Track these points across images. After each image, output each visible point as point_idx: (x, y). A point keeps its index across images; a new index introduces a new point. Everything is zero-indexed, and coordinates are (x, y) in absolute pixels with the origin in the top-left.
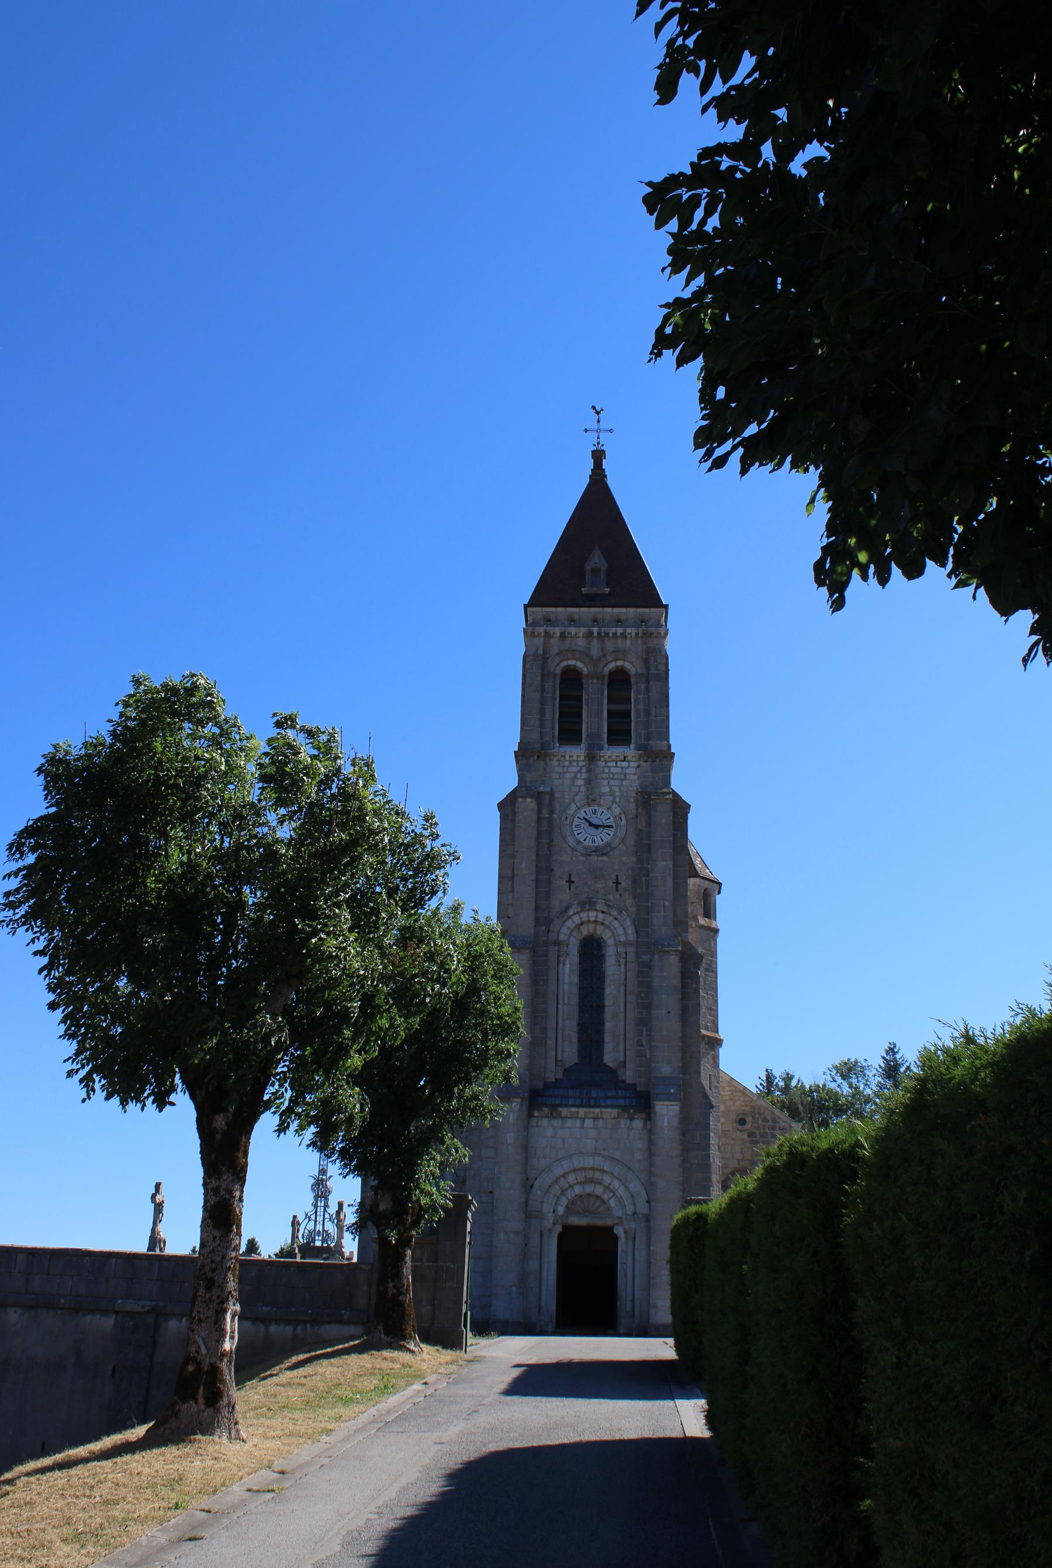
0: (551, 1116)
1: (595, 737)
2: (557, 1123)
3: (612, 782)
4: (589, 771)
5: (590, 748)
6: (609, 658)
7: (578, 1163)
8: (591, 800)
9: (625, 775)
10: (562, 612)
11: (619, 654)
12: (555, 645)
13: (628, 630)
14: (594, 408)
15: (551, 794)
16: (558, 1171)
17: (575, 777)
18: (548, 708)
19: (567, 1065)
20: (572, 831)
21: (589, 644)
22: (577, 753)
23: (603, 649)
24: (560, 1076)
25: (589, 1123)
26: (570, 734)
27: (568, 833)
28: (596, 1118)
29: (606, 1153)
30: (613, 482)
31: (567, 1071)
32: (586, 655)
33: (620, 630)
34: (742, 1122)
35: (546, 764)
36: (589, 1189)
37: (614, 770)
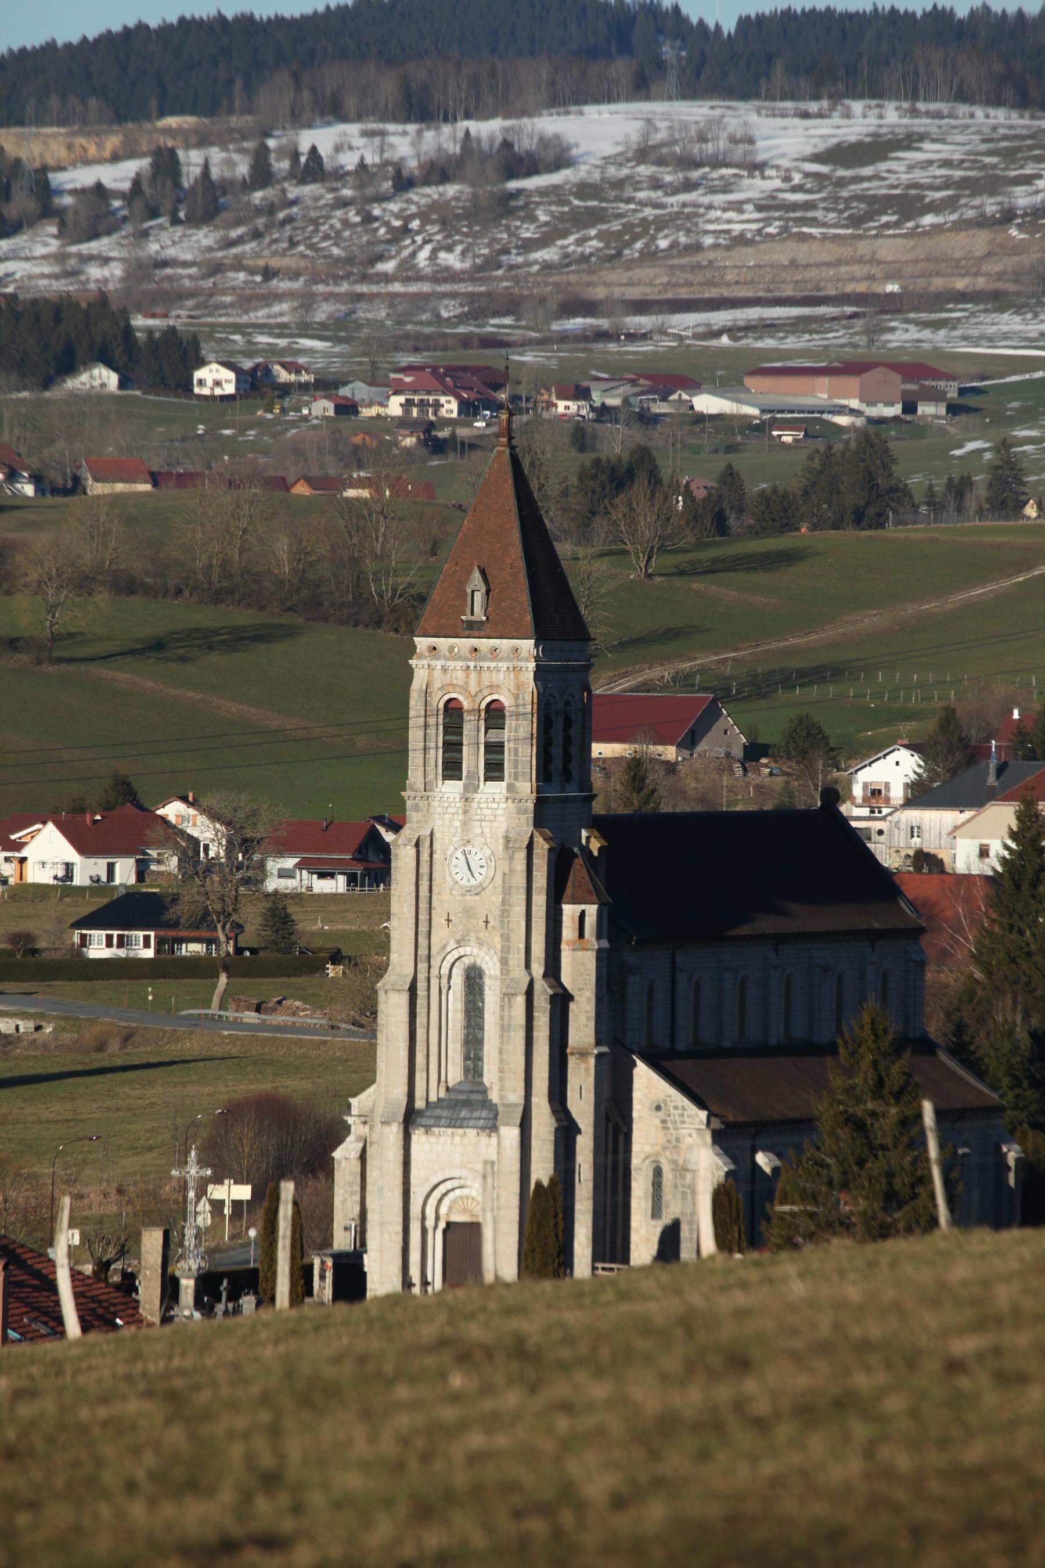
2: (432, 1139)
3: (483, 824)
4: (465, 812)
5: (466, 788)
6: (485, 692)
9: (495, 816)
11: (494, 687)
13: (500, 664)
17: (453, 819)
21: (467, 677)
23: (479, 682)
27: (447, 874)
29: (470, 1166)
33: (493, 665)
35: (429, 804)
37: (485, 812)
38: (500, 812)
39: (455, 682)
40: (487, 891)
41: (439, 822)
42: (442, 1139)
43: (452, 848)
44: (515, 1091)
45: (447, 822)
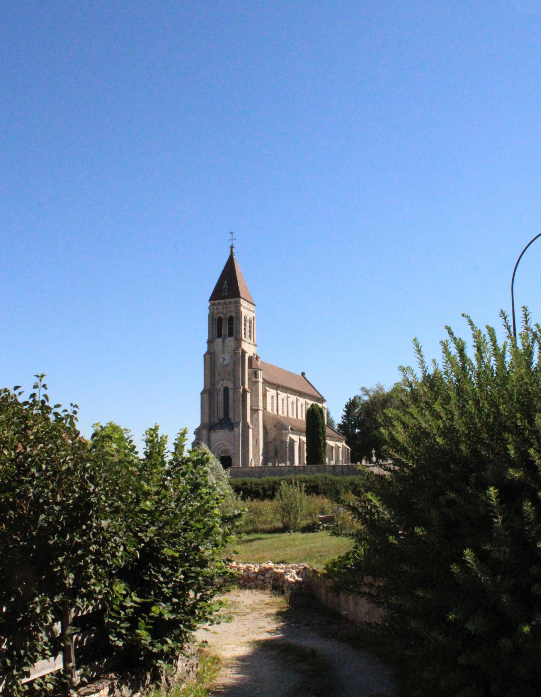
0: (215, 431)
1: (225, 335)
2: (216, 433)
4: (223, 345)
7: (220, 442)
8: (224, 353)
10: (217, 302)
12: (215, 311)
14: (231, 233)
15: (214, 352)
16: (216, 444)
18: (214, 329)
19: (221, 418)
22: (219, 340)
24: (218, 422)
25: (222, 433)
26: (219, 335)
28: (224, 432)
30: (235, 257)
31: (220, 420)
32: (223, 313)
34: (276, 426)
36: (225, 448)
38: (233, 344)
42: (218, 433)
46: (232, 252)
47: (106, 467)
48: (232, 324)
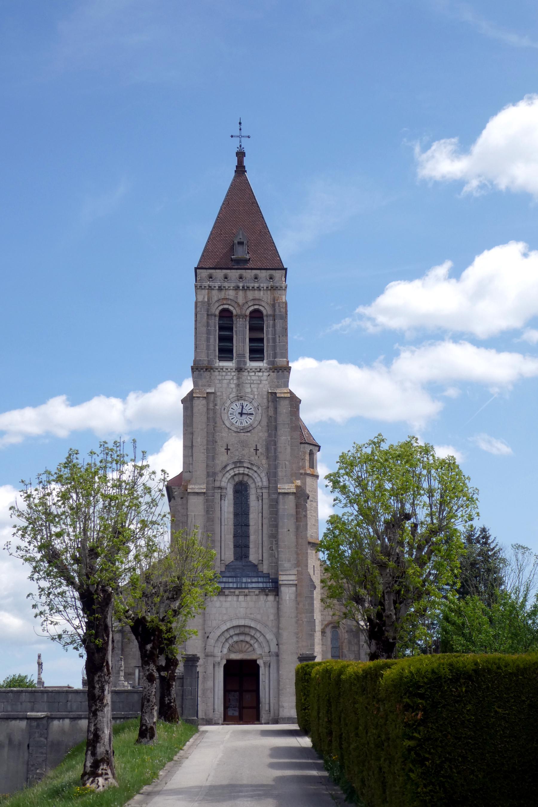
3: (252, 386)
4: (238, 378)
9: (261, 381)
18: (212, 337)
20: (228, 417)
37: (254, 378)
38: (265, 378)
39: (228, 297)
40: (256, 430)
41: (219, 385)
42: (230, 598)
43: (229, 402)
44: (289, 561)
45: (225, 385)
46: (240, 169)
47: (53, 570)
48: (261, 329)
